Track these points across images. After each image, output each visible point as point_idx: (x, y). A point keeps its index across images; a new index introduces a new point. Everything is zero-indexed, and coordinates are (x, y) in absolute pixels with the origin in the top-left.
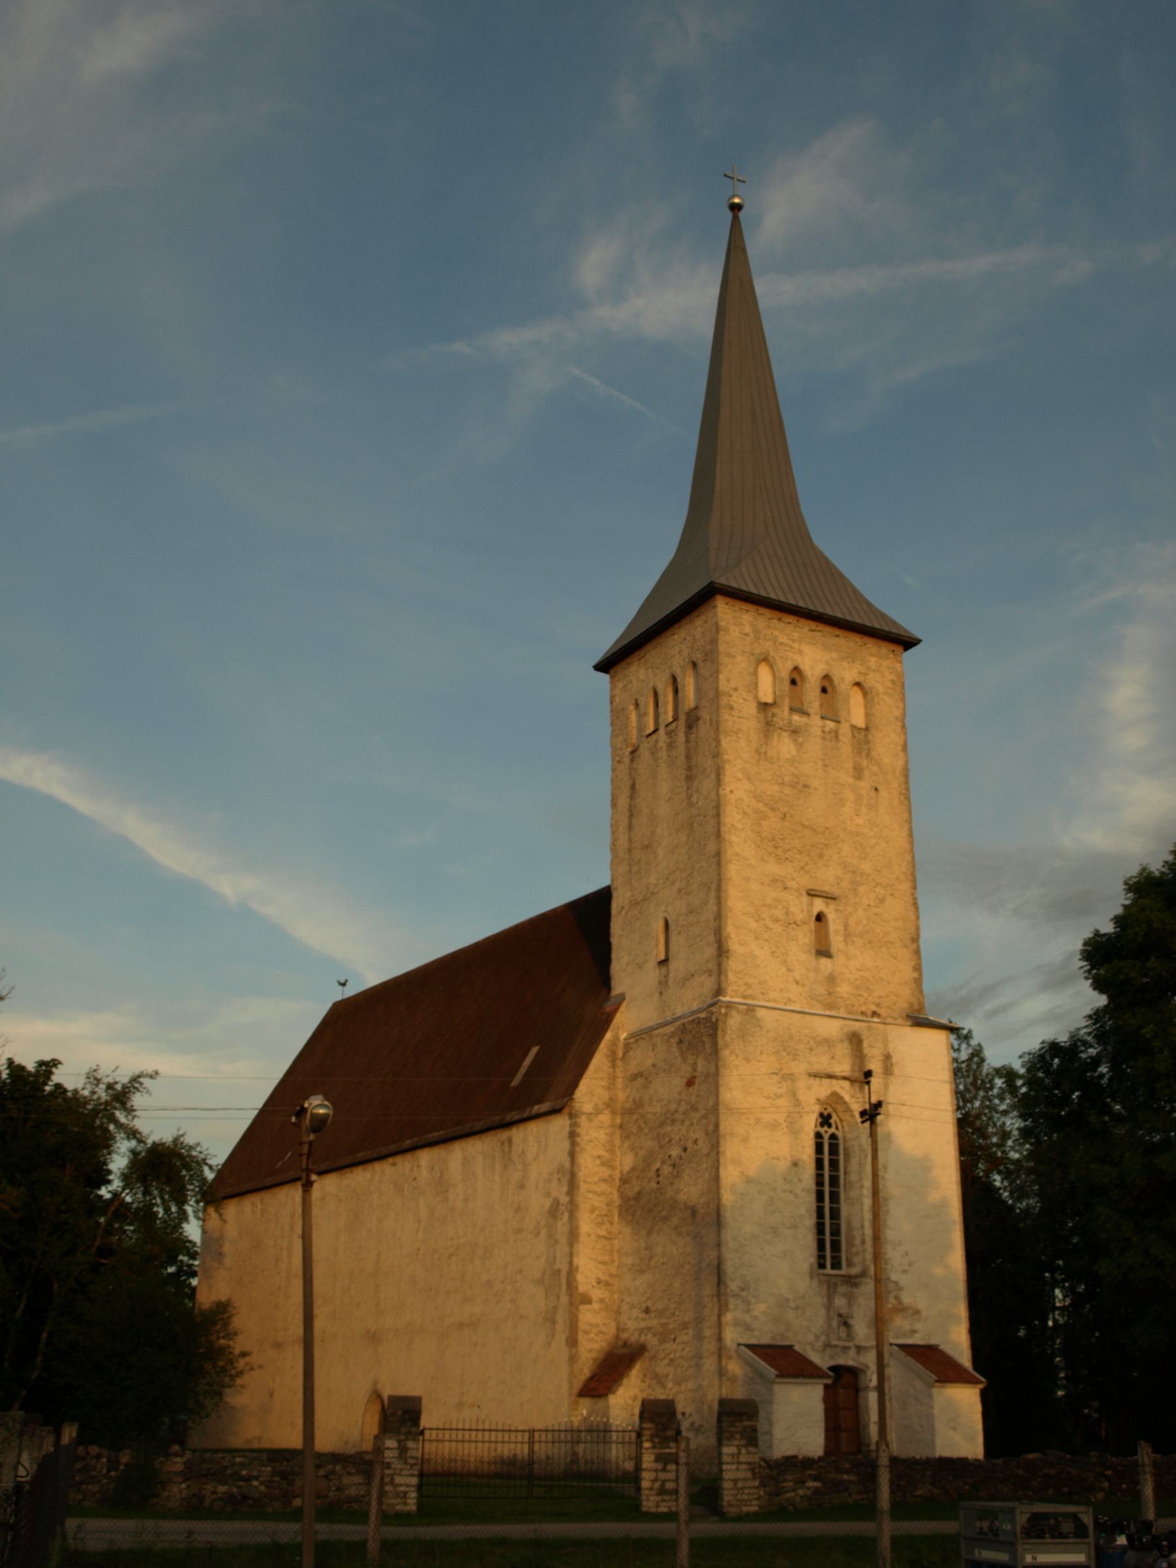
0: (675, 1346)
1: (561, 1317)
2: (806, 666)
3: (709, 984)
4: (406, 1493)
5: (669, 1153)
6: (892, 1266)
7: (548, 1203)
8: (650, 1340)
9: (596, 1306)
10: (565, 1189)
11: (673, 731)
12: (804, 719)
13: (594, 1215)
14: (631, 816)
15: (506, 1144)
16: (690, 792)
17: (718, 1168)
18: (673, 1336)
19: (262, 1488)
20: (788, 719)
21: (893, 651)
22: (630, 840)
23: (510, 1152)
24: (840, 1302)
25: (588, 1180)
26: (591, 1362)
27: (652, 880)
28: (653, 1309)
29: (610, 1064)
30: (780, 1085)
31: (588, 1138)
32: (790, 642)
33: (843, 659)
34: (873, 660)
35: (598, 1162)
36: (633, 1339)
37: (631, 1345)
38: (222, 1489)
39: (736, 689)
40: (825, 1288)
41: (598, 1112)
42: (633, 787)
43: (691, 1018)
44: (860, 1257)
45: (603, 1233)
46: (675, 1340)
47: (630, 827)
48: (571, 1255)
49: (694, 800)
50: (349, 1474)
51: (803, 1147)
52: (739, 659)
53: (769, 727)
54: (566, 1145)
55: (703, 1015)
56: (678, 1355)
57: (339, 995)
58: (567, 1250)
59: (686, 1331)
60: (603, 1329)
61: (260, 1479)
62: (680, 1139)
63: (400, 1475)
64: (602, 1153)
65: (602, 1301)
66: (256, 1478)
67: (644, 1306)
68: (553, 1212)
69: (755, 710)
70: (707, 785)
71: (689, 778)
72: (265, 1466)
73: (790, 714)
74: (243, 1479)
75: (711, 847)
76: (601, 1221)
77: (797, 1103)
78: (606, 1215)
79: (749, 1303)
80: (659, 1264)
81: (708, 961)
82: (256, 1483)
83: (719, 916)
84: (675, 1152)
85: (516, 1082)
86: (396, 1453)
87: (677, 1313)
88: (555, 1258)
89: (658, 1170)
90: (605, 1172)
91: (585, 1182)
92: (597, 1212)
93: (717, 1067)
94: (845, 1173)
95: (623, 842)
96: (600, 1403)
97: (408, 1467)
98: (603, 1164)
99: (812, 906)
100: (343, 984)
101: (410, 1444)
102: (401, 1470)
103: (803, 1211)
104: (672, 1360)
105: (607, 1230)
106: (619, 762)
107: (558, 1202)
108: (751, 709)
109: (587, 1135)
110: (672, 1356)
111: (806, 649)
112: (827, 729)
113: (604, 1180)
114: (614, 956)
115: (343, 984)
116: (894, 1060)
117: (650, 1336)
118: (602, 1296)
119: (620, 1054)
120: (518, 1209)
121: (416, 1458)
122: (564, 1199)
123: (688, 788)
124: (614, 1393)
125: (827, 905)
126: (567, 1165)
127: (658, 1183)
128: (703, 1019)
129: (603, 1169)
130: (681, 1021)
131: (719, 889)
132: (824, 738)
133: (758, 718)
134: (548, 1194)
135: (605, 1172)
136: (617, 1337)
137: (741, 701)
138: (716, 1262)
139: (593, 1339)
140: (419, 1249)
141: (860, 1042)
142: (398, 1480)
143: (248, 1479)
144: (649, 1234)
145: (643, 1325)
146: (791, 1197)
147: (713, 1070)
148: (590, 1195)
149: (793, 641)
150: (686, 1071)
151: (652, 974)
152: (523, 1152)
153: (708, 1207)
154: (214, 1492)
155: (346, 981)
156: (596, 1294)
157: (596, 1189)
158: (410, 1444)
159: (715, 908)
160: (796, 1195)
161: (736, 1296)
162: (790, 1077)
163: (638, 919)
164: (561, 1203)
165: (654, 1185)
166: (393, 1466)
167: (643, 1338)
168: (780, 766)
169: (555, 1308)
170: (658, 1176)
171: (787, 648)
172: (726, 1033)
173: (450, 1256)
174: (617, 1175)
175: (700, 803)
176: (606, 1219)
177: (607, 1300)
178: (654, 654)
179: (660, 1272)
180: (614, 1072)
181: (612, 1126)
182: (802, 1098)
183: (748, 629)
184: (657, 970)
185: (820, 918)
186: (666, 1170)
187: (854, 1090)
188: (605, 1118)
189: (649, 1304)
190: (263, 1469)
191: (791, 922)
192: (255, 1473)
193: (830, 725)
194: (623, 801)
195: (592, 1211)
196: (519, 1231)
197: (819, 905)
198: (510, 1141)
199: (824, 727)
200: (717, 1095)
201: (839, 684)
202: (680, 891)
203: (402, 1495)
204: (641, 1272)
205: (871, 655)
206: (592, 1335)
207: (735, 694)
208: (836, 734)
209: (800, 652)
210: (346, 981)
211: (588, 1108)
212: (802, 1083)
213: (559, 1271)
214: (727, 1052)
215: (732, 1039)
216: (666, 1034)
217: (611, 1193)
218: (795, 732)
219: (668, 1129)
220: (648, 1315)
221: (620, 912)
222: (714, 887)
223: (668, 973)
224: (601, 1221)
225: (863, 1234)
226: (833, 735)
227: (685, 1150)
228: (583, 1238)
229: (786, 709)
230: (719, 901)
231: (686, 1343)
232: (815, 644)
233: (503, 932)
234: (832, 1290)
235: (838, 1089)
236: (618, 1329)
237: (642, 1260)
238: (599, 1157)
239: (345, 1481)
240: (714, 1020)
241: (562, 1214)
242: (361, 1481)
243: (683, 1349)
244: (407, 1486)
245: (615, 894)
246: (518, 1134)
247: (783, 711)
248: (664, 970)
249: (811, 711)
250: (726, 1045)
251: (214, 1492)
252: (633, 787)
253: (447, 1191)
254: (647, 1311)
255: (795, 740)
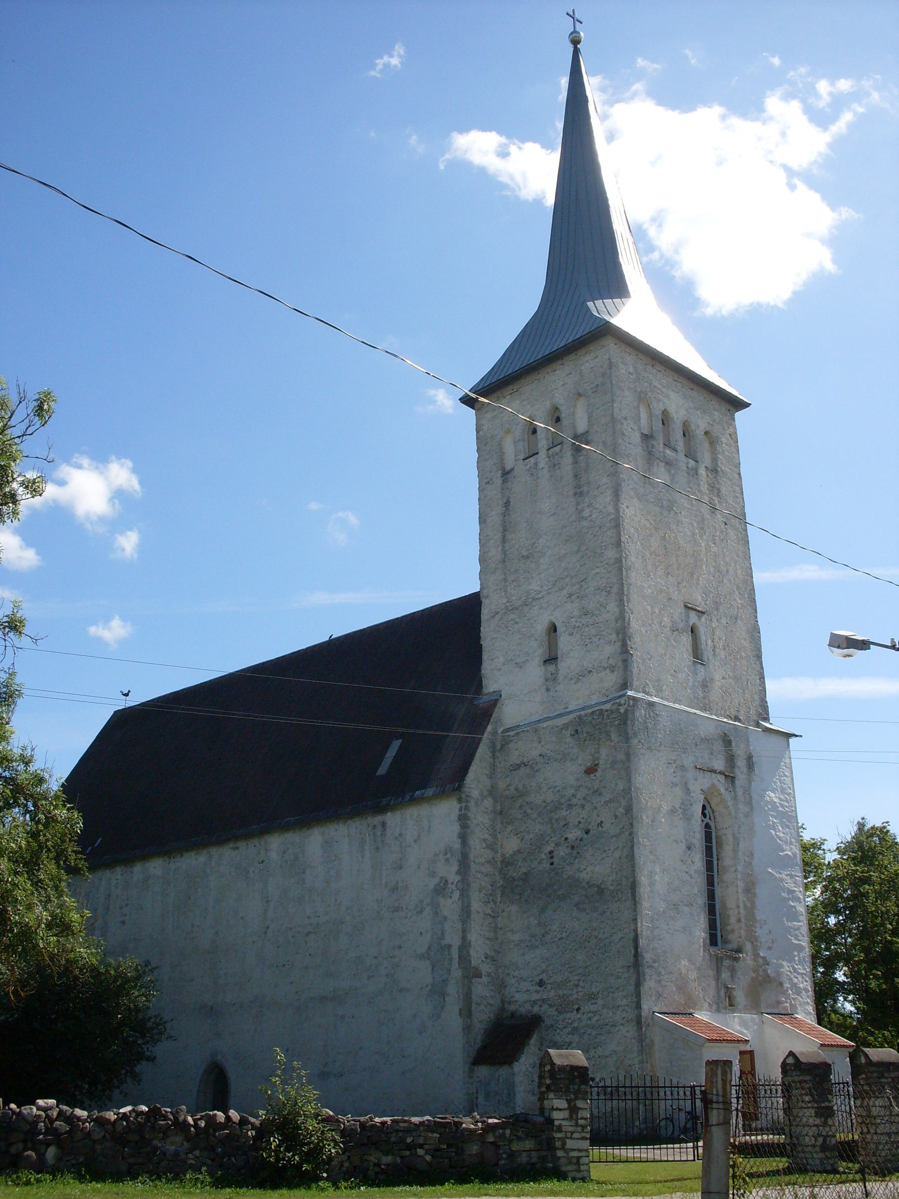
0: (579, 1016)
1: (453, 990)
2: (672, 410)
3: (611, 680)
4: (578, 1158)
5: (566, 836)
6: (761, 943)
7: (433, 882)
8: (547, 1012)
9: (485, 979)
10: (455, 868)
11: (557, 454)
12: (674, 454)
13: (482, 895)
14: (505, 530)
15: (379, 828)
16: (580, 507)
17: (632, 847)
18: (576, 1007)
19: (428, 1158)
20: (663, 452)
21: (729, 410)
22: (504, 552)
23: (383, 835)
24: (725, 975)
25: (477, 861)
26: (482, 1031)
27: (534, 586)
28: (551, 981)
29: (491, 755)
30: (675, 775)
31: (476, 822)
32: (661, 387)
33: (697, 409)
34: (716, 413)
35: (484, 845)
36: (523, 1010)
37: (521, 1015)
38: (387, 1159)
39: (626, 419)
40: (714, 961)
41: (483, 797)
42: (507, 504)
43: (590, 711)
44: (737, 934)
45: (489, 911)
46: (578, 1010)
47: (504, 540)
48: (464, 931)
49: (586, 513)
50: (519, 1139)
51: (694, 832)
52: (627, 393)
53: (650, 456)
54: (456, 828)
55: (607, 706)
56: (583, 1024)
57: (122, 704)
58: (459, 926)
59: (594, 1001)
60: (491, 1002)
61: (426, 1147)
62: (579, 822)
63: (571, 1138)
64: (486, 836)
65: (489, 975)
66: (421, 1146)
67: (537, 979)
68: (441, 889)
69: (639, 440)
70: (605, 500)
71: (579, 494)
72: (433, 1132)
73: (664, 448)
74: (409, 1147)
75: (611, 554)
76: (487, 900)
77: (687, 791)
78: (491, 895)
79: (660, 974)
80: (556, 939)
81: (609, 658)
82: (420, 1152)
83: (622, 616)
84: (573, 834)
85: (382, 770)
86: (566, 1114)
87: (581, 984)
88: (443, 934)
89: (551, 852)
90: (489, 854)
91: (474, 862)
92: (484, 891)
93: (628, 755)
94: (718, 860)
95: (495, 553)
96: (503, 1071)
97: (579, 1129)
98: (487, 847)
99: (688, 618)
100: (127, 695)
101: (580, 1104)
102: (572, 1133)
103: (696, 891)
104: (575, 1029)
105: (492, 908)
106: (488, 483)
107: (446, 881)
108: (636, 438)
109: (475, 818)
110: (575, 1025)
111: (672, 395)
112: (690, 466)
113: (489, 862)
114: (485, 657)
115: (127, 695)
116: (754, 759)
117: (545, 1007)
118: (490, 970)
119: (499, 746)
120: (395, 888)
121: (586, 1119)
122: (453, 878)
123: (578, 504)
124: (517, 1060)
125: (700, 618)
126: (457, 846)
127: (552, 864)
128: (607, 711)
129: (488, 851)
130: (578, 714)
131: (621, 592)
132: (688, 473)
133: (642, 447)
134: (433, 874)
135: (489, 854)
136: (502, 1009)
137: (630, 430)
138: (632, 935)
139: (483, 1010)
140: (268, 927)
141: (730, 742)
142: (570, 1144)
143: (411, 1147)
144: (543, 910)
145: (535, 997)
146: (687, 877)
147: (621, 756)
148: (479, 876)
149: (663, 387)
150: (585, 759)
151: (535, 672)
152: (401, 834)
153: (620, 884)
154: (378, 1165)
155: (129, 691)
156: (485, 968)
157: (484, 870)
158: (580, 1104)
159: (617, 610)
160: (691, 875)
161: (650, 967)
162: (683, 768)
163: (516, 623)
164: (450, 881)
165: (548, 866)
166: (564, 1129)
167: (536, 1009)
168: (659, 492)
169: (445, 981)
170: (552, 857)
171: (659, 392)
172: (634, 724)
173: (308, 934)
174: (499, 858)
175: (594, 516)
176: (491, 898)
177: (493, 974)
178: (528, 387)
179: (558, 947)
180: (494, 762)
181: (494, 812)
182: (691, 787)
183: (631, 370)
184: (543, 668)
185: (693, 630)
186: (562, 851)
187: (728, 784)
188: (488, 803)
189: (544, 977)
190: (430, 1135)
191: (674, 629)
192: (421, 1141)
193: (692, 463)
194: (495, 517)
195: (480, 890)
196: (397, 909)
197: (693, 618)
198: (384, 824)
199: (688, 463)
200: (629, 780)
201: (695, 430)
202: (570, 595)
203: (574, 1161)
204: (533, 947)
205: (715, 410)
206: (482, 1007)
207: (625, 423)
208: (696, 471)
209: (668, 397)
210: (129, 691)
211: (475, 793)
212: (691, 774)
213: (450, 946)
214: (635, 741)
215: (639, 729)
216: (557, 727)
217: (494, 875)
218: (668, 463)
219: (564, 813)
220: (543, 988)
221: (493, 617)
222: (615, 590)
223: (557, 670)
224: (487, 900)
225: (739, 913)
226: (694, 471)
227: (587, 832)
228: (474, 916)
229: (661, 445)
230: (621, 603)
231: (593, 1012)
232: (678, 393)
233: (190, 688)
234: (719, 964)
235: (715, 782)
236: (503, 1002)
237: (533, 936)
238: (485, 840)
239: (515, 1147)
240: (622, 711)
241: (452, 893)
242: (532, 1146)
243: (590, 1019)
244: (580, 1150)
245: (485, 602)
246: (393, 819)
247: (659, 444)
248: (551, 668)
249: (679, 449)
250: (635, 734)
251: (378, 1165)
252: (507, 504)
253: (304, 873)
254: (541, 983)
255: (669, 472)
